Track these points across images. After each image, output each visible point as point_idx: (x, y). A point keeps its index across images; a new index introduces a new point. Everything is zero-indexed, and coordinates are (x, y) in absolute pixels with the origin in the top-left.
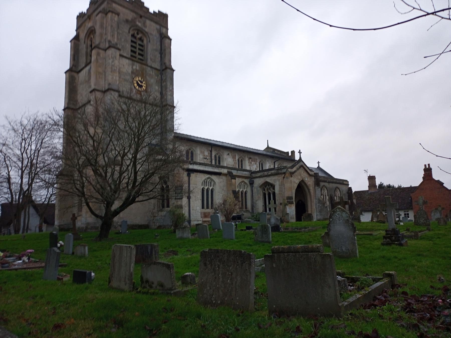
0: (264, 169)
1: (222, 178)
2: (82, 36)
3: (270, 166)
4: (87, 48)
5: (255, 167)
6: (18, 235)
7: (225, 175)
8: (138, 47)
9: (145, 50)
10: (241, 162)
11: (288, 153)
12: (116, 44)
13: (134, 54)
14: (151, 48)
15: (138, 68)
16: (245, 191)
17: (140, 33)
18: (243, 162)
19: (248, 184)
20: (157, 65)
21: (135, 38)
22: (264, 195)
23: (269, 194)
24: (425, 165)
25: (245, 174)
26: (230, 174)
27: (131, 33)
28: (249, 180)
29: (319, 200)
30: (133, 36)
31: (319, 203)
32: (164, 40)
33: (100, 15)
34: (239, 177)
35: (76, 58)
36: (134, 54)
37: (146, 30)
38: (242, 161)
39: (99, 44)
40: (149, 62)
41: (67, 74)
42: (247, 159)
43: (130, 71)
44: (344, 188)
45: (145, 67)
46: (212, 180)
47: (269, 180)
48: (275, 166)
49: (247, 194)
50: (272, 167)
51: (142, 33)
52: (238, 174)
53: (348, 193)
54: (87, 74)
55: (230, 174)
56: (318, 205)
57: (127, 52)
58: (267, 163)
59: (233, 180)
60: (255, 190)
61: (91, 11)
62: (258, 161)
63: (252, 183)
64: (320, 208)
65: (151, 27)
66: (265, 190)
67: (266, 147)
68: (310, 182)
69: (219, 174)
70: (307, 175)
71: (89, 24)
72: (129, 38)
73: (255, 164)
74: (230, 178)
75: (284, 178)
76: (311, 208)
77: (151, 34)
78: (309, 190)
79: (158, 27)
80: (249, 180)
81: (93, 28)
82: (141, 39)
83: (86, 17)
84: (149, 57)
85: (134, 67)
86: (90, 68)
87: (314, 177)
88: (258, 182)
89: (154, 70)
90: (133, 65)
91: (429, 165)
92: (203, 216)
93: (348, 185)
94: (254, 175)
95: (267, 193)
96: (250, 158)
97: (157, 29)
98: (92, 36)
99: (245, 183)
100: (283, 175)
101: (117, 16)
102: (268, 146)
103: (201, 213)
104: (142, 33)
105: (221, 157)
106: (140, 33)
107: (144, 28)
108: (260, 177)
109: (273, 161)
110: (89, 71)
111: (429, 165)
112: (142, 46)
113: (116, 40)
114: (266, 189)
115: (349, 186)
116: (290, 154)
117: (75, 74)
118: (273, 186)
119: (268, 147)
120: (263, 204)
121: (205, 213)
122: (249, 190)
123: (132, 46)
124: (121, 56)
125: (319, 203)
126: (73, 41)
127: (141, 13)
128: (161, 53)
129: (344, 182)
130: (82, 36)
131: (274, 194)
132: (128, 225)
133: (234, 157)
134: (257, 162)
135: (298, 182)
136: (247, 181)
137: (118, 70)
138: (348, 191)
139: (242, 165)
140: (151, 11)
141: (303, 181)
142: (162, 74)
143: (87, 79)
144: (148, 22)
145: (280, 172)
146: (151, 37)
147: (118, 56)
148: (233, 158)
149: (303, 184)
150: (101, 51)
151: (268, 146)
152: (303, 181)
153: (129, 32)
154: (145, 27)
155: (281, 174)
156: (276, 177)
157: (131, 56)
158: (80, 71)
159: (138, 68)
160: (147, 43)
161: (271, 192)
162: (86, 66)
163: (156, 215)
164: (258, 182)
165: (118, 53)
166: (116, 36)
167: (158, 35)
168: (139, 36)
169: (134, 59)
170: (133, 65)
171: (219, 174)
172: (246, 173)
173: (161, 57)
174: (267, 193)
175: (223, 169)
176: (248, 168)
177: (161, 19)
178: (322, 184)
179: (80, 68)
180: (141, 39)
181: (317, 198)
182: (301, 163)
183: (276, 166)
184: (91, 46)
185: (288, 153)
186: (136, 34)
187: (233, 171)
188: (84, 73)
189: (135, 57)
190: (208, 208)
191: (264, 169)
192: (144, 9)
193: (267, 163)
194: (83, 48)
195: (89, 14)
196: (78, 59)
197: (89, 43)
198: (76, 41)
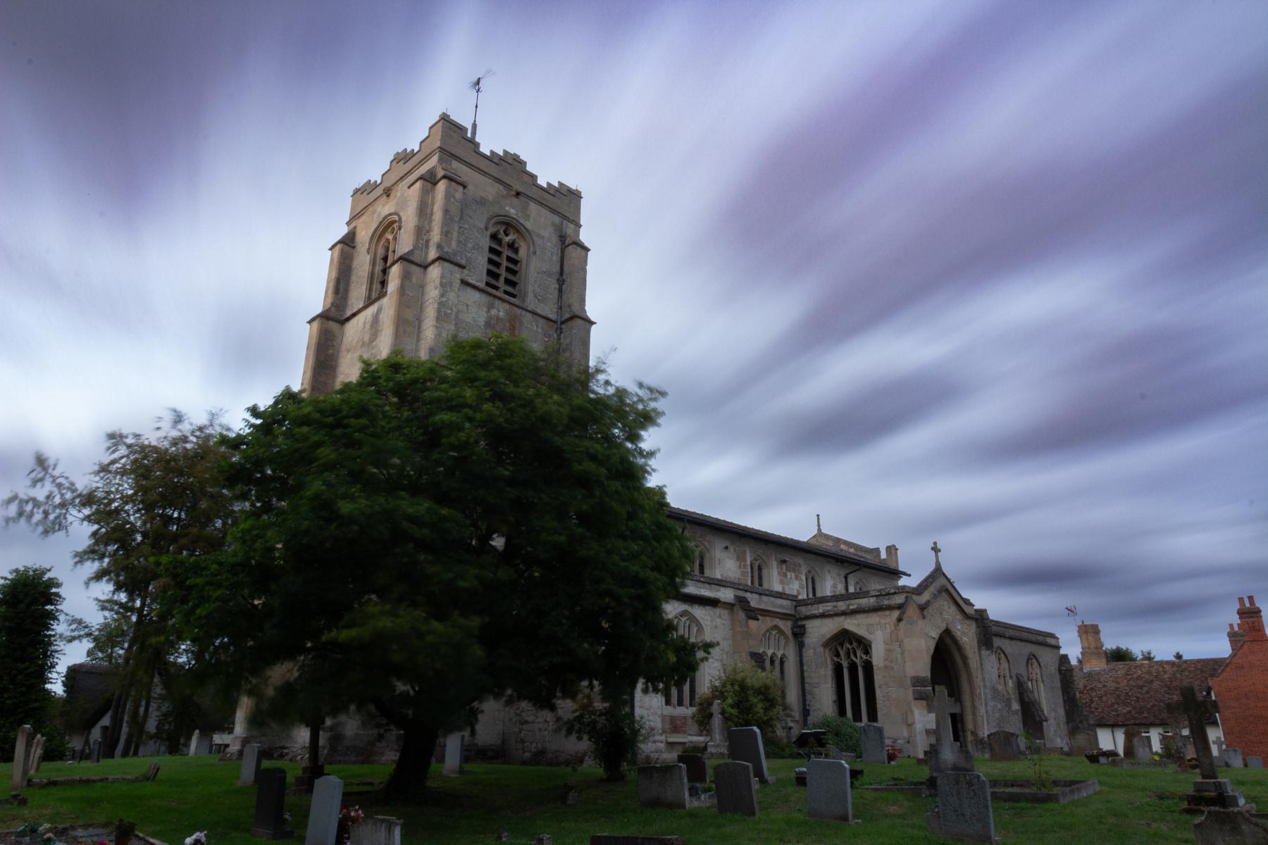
0: (819, 594)
1: (720, 617)
2: (364, 236)
3: (835, 586)
4: (374, 263)
5: (796, 587)
6: (177, 758)
7: (730, 606)
8: (505, 263)
9: (523, 271)
10: (758, 572)
11: (877, 550)
12: (455, 255)
13: (493, 282)
14: (537, 268)
15: (501, 314)
16: (779, 654)
17: (511, 231)
18: (765, 572)
19: (790, 636)
20: (549, 310)
21: (499, 242)
22: (838, 670)
23: (853, 668)
24: (1241, 600)
25: (781, 606)
26: (742, 603)
27: (492, 230)
28: (789, 623)
29: (994, 689)
30: (494, 237)
31: (994, 698)
32: (570, 251)
33: (418, 185)
34: (766, 613)
35: (341, 286)
36: (493, 282)
37: (528, 225)
38: (760, 569)
39: (411, 252)
40: (531, 302)
41: (315, 324)
42: (775, 564)
43: (481, 321)
44: (1046, 657)
45: (518, 311)
46: (693, 619)
47: (851, 624)
48: (847, 589)
49: (786, 665)
50: (840, 589)
51: (518, 231)
52: (762, 606)
53: (1060, 671)
54: (368, 326)
55: (742, 603)
56: (991, 704)
57: (479, 276)
58: (828, 577)
59: (752, 623)
60: (809, 653)
61: (394, 177)
62: (804, 570)
63: (799, 634)
64: (997, 715)
65: (538, 221)
66: (838, 655)
67: (815, 532)
68: (966, 635)
69: (713, 603)
70: (959, 617)
71: (385, 208)
72: (486, 242)
73: (797, 577)
74: (741, 615)
75: (900, 620)
76: (974, 714)
77: (539, 235)
78: (964, 658)
79: (557, 219)
80: (789, 623)
81: (396, 218)
82: (512, 246)
83: (379, 191)
84: (530, 289)
85: (494, 312)
86: (379, 311)
87: (976, 620)
88: (819, 631)
89: (541, 321)
90: (490, 307)
91: (1251, 598)
92: (668, 726)
93: (1058, 648)
94: (804, 611)
95: (845, 664)
96: (784, 562)
97: (553, 224)
98: (390, 237)
99: (781, 632)
100: (896, 613)
101: (461, 188)
102: (819, 530)
103: (663, 717)
104: (518, 231)
105: (707, 555)
106: (511, 231)
107: (522, 221)
108: (823, 616)
109: (843, 573)
110: (376, 319)
111: (1251, 598)
112: (515, 262)
113: (454, 244)
114: (842, 653)
115: (1062, 652)
116: (883, 555)
117: (333, 326)
118: (866, 646)
119: (820, 533)
120: (834, 698)
121: (673, 719)
122: (791, 653)
123: (490, 261)
124: (465, 283)
125: (994, 698)
126: (338, 247)
127: (518, 186)
128: (561, 282)
129: (1049, 640)
130: (364, 236)
131: (868, 667)
132: (1105, 652)
133: (740, 558)
134: (800, 573)
135: (935, 634)
136: (786, 626)
137: (453, 316)
138: (1060, 665)
139: (760, 578)
140: (542, 182)
141: (947, 633)
142: (560, 331)
143: (367, 338)
144: (533, 207)
145: (886, 602)
146: (538, 241)
147: (457, 284)
148: (738, 558)
149: (948, 641)
150: (414, 268)
151: (819, 530)
152: (947, 633)
153: (487, 229)
154: (527, 217)
155: (890, 608)
156: (873, 618)
157: (488, 284)
158: (348, 319)
159: (501, 314)
160: (528, 255)
161: (858, 661)
162: (365, 307)
163: (530, 719)
164: (819, 631)
165: (458, 274)
166: (455, 234)
167: (555, 239)
168: (507, 239)
169: (494, 291)
170: (490, 307)
171: (713, 603)
172: (784, 602)
173: (560, 290)
174: (845, 664)
175: (722, 589)
176: (777, 587)
177: (564, 202)
178: (997, 642)
179: (349, 313)
180: (512, 246)
181: (988, 684)
182: (943, 581)
183: (851, 590)
184: (385, 259)
185: (877, 550)
186: (501, 235)
187: (748, 595)
188: (361, 325)
189: (496, 288)
190: (680, 703)
191: (819, 594)
192: (526, 178)
193: (828, 577)
194: (363, 262)
195: (387, 184)
196: (347, 291)
197: (381, 252)
198: (347, 248)
